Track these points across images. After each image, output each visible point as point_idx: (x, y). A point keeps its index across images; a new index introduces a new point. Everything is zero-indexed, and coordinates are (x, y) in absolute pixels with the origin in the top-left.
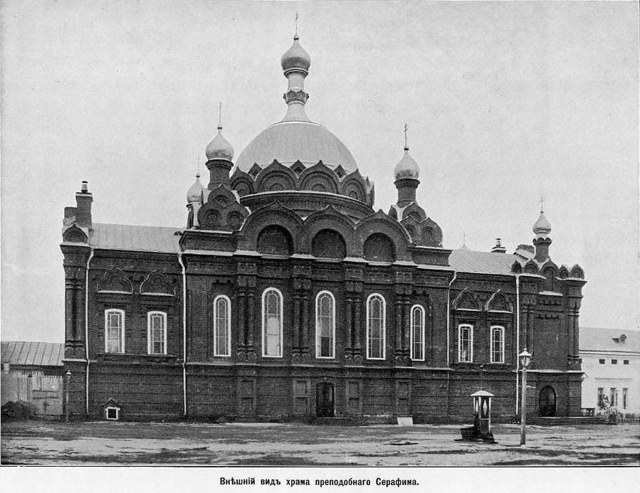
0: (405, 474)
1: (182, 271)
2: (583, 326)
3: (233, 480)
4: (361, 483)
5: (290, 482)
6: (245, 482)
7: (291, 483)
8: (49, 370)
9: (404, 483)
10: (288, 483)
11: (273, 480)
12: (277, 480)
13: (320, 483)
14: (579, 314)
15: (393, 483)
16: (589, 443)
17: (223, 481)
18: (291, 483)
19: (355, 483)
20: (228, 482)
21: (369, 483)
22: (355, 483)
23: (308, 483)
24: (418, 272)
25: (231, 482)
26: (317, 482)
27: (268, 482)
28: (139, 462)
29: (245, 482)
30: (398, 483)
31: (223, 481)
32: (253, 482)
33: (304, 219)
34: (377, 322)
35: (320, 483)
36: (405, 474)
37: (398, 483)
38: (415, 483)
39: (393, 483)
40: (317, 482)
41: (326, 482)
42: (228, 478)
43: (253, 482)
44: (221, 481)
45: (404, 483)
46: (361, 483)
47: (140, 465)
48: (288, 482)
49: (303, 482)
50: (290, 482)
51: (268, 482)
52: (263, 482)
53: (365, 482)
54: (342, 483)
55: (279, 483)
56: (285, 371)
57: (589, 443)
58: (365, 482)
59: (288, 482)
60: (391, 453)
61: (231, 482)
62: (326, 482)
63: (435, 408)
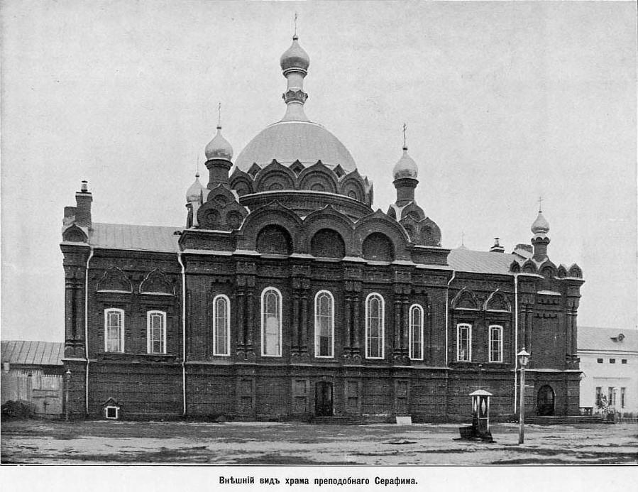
0: (403, 473)
1: (181, 270)
2: (581, 325)
3: (232, 479)
4: (360, 482)
5: (289, 481)
6: (244, 481)
7: (290, 482)
8: (49, 370)
9: (403, 482)
10: (287, 482)
11: (272, 479)
12: (276, 479)
13: (319, 482)
14: (577, 313)
15: (392, 482)
16: (587, 442)
17: (222, 480)
18: (290, 482)
19: (354, 482)
20: (227, 481)
21: (367, 482)
22: (354, 482)
23: (307, 482)
24: (416, 272)
25: (230, 481)
26: (316, 481)
27: (267, 481)
28: (138, 461)
29: (244, 481)
30: (397, 482)
31: (222, 480)
32: (252, 481)
33: (303, 218)
34: (376, 322)
35: (319, 482)
36: (403, 473)
37: (397, 482)
38: (413, 482)
39: (392, 482)
40: (316, 481)
41: (325, 481)
42: (227, 477)
43: (252, 481)
44: (221, 480)
45: (403, 482)
46: (360, 482)
47: (139, 464)
48: (287, 481)
49: (302, 481)
50: (289, 481)
51: (267, 481)
52: (262, 481)
53: (364, 481)
54: (341, 482)
55: (278, 482)
56: (284, 370)
57: (587, 442)
58: (364, 481)
59: (287, 481)
60: (390, 452)
61: (230, 481)
62: (325, 481)
63: (434, 407)
